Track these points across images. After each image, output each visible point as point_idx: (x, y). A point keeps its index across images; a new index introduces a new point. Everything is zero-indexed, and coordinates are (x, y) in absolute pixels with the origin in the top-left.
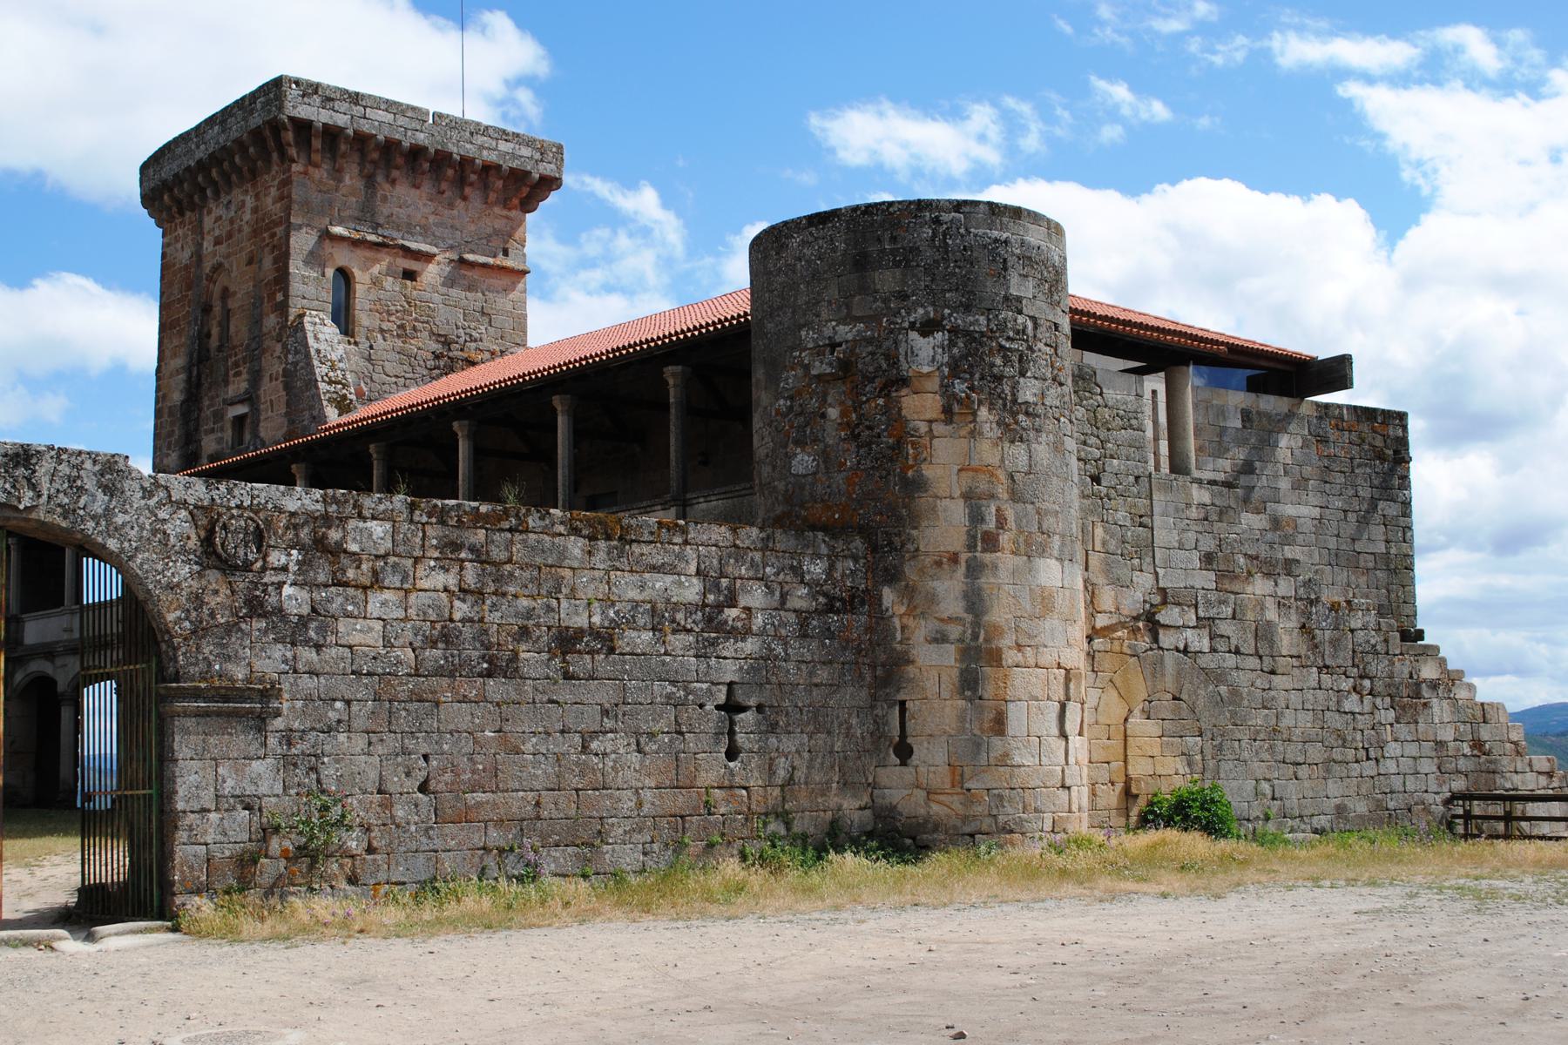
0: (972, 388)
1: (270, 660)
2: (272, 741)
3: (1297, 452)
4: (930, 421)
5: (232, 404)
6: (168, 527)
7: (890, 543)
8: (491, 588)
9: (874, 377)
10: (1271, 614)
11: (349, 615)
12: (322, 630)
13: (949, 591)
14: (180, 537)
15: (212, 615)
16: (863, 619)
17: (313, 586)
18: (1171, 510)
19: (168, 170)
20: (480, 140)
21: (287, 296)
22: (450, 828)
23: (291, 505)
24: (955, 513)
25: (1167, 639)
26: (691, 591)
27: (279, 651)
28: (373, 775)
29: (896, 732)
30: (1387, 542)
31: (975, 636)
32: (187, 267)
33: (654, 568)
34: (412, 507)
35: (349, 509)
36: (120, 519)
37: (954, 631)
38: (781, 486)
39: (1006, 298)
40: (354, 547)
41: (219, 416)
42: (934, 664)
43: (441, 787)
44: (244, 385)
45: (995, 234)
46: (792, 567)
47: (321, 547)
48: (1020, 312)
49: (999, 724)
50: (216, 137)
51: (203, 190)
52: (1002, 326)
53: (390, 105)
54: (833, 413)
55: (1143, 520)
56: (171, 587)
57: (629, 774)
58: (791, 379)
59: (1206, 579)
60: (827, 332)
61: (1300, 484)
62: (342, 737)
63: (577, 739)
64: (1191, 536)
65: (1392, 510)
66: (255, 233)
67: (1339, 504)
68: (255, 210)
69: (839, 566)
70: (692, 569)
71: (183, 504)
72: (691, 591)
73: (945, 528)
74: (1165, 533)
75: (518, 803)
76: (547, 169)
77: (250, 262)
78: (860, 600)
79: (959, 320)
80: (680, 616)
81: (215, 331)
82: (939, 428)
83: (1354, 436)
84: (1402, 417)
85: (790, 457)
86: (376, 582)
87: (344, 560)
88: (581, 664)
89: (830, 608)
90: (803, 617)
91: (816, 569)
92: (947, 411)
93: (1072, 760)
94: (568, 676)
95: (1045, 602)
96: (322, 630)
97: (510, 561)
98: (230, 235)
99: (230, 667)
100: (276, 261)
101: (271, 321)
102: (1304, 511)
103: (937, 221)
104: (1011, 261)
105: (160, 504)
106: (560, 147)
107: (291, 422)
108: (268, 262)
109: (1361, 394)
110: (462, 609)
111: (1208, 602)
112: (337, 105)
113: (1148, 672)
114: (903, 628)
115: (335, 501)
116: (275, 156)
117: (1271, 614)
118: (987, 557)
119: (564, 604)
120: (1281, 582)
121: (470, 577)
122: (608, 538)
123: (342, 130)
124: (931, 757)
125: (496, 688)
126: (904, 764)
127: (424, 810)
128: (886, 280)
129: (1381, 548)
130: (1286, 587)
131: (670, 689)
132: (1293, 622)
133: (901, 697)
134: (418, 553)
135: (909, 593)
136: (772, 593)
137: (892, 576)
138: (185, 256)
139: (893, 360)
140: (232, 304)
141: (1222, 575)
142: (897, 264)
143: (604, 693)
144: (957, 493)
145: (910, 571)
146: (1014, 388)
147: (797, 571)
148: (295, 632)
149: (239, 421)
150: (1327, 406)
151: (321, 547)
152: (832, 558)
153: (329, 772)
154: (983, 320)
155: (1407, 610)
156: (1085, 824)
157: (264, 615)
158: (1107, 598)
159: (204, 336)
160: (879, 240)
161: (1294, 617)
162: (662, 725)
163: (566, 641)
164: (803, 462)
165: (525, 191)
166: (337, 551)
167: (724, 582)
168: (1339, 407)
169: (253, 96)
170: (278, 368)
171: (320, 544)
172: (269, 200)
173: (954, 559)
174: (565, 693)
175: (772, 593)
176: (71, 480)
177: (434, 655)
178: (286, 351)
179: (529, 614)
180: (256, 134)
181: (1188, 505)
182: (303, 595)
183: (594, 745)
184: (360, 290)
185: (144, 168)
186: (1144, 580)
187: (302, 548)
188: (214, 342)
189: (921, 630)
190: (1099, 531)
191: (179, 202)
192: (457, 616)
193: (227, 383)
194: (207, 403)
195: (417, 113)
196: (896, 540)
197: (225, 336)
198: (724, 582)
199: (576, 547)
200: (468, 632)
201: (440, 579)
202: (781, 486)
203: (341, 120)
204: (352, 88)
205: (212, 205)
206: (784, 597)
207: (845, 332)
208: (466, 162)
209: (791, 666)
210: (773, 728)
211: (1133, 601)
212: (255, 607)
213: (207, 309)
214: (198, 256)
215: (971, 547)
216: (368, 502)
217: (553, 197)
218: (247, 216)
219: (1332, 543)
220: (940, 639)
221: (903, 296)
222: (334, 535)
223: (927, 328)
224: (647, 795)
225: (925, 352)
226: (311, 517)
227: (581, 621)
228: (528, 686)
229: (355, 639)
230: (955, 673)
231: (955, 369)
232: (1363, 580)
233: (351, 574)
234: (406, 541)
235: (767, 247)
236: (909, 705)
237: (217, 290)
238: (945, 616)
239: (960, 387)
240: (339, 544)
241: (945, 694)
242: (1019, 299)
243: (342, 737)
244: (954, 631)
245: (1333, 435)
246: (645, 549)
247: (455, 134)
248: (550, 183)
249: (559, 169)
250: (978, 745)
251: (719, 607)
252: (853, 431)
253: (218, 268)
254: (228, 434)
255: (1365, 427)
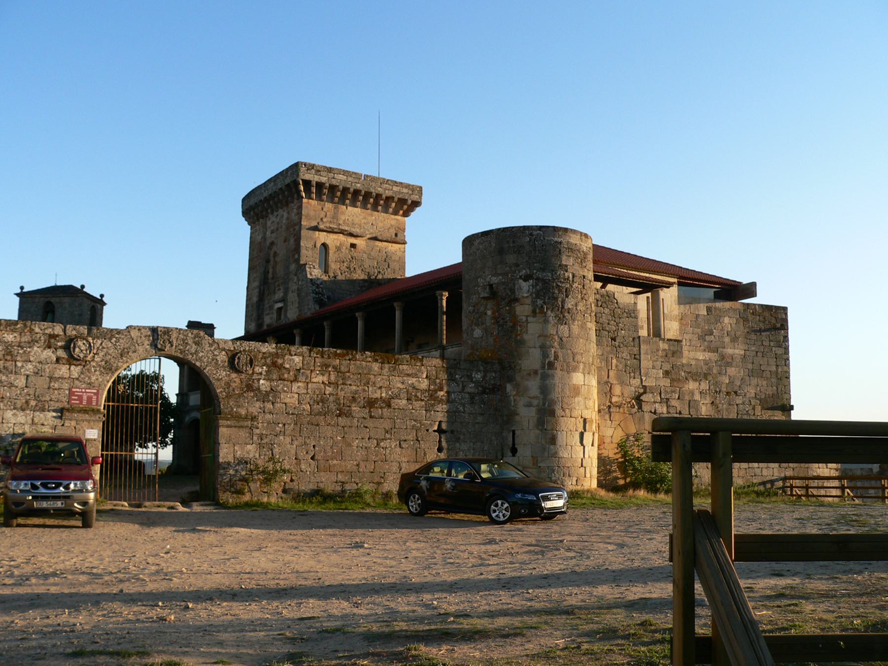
0: (544, 303)
1: (255, 408)
2: (255, 438)
3: (733, 325)
4: (527, 316)
5: (277, 302)
6: (218, 358)
7: (510, 366)
8: (341, 382)
9: (502, 297)
10: (697, 397)
11: (285, 391)
12: (275, 397)
13: (533, 386)
14: (222, 361)
15: (234, 390)
16: (499, 397)
17: (271, 380)
18: (649, 352)
19: (253, 201)
20: (385, 186)
21: (299, 256)
22: (322, 474)
23: (264, 350)
24: (536, 353)
25: (646, 408)
26: (424, 384)
27: (258, 404)
28: (293, 452)
29: (511, 443)
30: (777, 366)
31: (544, 404)
32: (260, 243)
33: (408, 375)
34: (310, 351)
35: (286, 351)
36: (201, 354)
37: (535, 402)
38: (470, 342)
39: (560, 265)
40: (287, 366)
41: (271, 307)
42: (526, 415)
43: (319, 458)
44: (282, 294)
45: (556, 239)
46: (468, 376)
47: (275, 366)
48: (567, 271)
49: (553, 440)
50: (272, 188)
51: (267, 210)
52: (558, 278)
53: (345, 173)
54: (489, 313)
55: (637, 357)
56: (218, 380)
57: (397, 456)
58: (474, 299)
59: (666, 382)
60: (488, 279)
61: (734, 339)
62: (281, 438)
63: (375, 441)
64: (659, 363)
65: (780, 351)
66: (288, 229)
67: (753, 348)
68: (288, 219)
69: (488, 375)
70: (425, 376)
71: (224, 349)
72: (424, 384)
73: (531, 360)
74: (646, 363)
75: (350, 465)
76: (415, 197)
77: (285, 241)
78: (497, 389)
79: (540, 275)
80: (419, 394)
81: (271, 271)
82: (530, 319)
83: (761, 319)
84: (785, 309)
85: (473, 330)
86: (296, 380)
87: (284, 371)
88: (377, 412)
89: (484, 392)
90: (472, 396)
91: (478, 376)
92: (534, 312)
93: (586, 456)
94: (371, 417)
95: (576, 391)
96: (275, 397)
97: (349, 372)
98: (277, 229)
99: (240, 410)
100: (295, 240)
101: (293, 267)
102: (737, 351)
103: (531, 234)
104: (563, 250)
105: (215, 349)
106: (421, 188)
107: (300, 311)
108: (292, 241)
109: (762, 298)
110: (329, 390)
111: (666, 391)
112: (322, 173)
113: (636, 421)
114: (515, 400)
115: (280, 348)
116: (296, 196)
117: (697, 397)
118: (550, 372)
119: (370, 389)
120: (702, 383)
121: (333, 378)
122: (389, 363)
123: (324, 184)
124: (525, 453)
125: (342, 421)
126: (514, 455)
127: (312, 466)
128: (511, 259)
129: (774, 368)
130: (704, 386)
131: (414, 423)
132: (708, 400)
133: (513, 428)
134: (312, 368)
135: (517, 386)
136: (458, 385)
137: (510, 380)
138: (259, 238)
139: (513, 291)
140: (278, 259)
141: (672, 380)
142: (515, 252)
143: (387, 424)
144: (537, 345)
145: (518, 378)
146: (563, 302)
147: (470, 377)
148: (264, 397)
149: (280, 309)
150: (748, 304)
151: (275, 366)
152: (486, 372)
153: (276, 450)
154: (550, 274)
155: (786, 396)
156: (594, 484)
157: (253, 391)
158: (617, 390)
159: (266, 273)
160: (508, 242)
161: (708, 398)
162: (410, 437)
163: (371, 403)
164: (478, 332)
165: (405, 207)
166: (281, 367)
167: (438, 381)
168: (754, 305)
169: (287, 170)
170: (295, 287)
171: (274, 364)
172: (293, 215)
173: (536, 372)
174: (370, 423)
175: (458, 385)
176: (183, 340)
177: (318, 407)
178: (298, 280)
179: (356, 392)
180: (288, 185)
181: (658, 350)
182: (268, 384)
183: (382, 444)
184: (331, 252)
185: (244, 200)
186: (636, 382)
187: (268, 366)
188: (270, 275)
189: (522, 401)
190: (614, 361)
191: (257, 215)
192: (327, 392)
193: (275, 293)
194: (266, 302)
195: (357, 176)
196: (513, 365)
197: (274, 273)
198: (438, 381)
199: (376, 367)
200: (331, 399)
201: (320, 379)
202: (470, 342)
203: (323, 179)
204: (328, 166)
205: (270, 216)
206: (464, 387)
207: (495, 280)
208: (378, 196)
209: (466, 416)
210: (458, 440)
211: (630, 391)
212: (249, 388)
213: (268, 261)
214: (264, 238)
215: (543, 367)
216: (293, 349)
217: (418, 209)
218: (284, 221)
219: (750, 366)
220: (529, 405)
221: (517, 265)
222: (280, 361)
223: (526, 279)
224: (404, 465)
225: (525, 287)
226: (271, 354)
227: (377, 395)
228: (355, 421)
229: (287, 400)
230: (535, 419)
231: (538, 296)
232: (765, 383)
233: (286, 376)
234: (308, 364)
235: (469, 243)
236: (517, 432)
237: (272, 252)
238: (532, 395)
239: (539, 302)
240: (282, 365)
241: (531, 427)
242: (566, 266)
243: (281, 438)
244: (535, 402)
245: (750, 317)
246: (405, 367)
247: (373, 184)
248: (416, 204)
249: (420, 197)
250: (544, 449)
251: (436, 391)
252: (496, 320)
253: (272, 243)
254: (275, 316)
255: (767, 314)
